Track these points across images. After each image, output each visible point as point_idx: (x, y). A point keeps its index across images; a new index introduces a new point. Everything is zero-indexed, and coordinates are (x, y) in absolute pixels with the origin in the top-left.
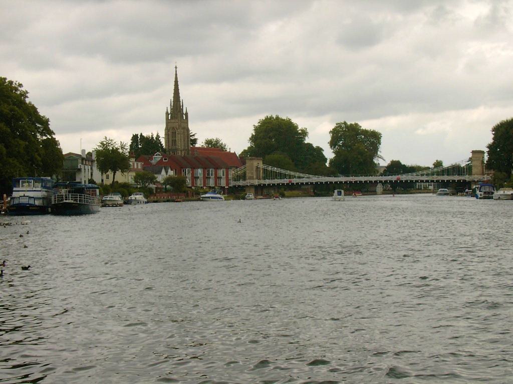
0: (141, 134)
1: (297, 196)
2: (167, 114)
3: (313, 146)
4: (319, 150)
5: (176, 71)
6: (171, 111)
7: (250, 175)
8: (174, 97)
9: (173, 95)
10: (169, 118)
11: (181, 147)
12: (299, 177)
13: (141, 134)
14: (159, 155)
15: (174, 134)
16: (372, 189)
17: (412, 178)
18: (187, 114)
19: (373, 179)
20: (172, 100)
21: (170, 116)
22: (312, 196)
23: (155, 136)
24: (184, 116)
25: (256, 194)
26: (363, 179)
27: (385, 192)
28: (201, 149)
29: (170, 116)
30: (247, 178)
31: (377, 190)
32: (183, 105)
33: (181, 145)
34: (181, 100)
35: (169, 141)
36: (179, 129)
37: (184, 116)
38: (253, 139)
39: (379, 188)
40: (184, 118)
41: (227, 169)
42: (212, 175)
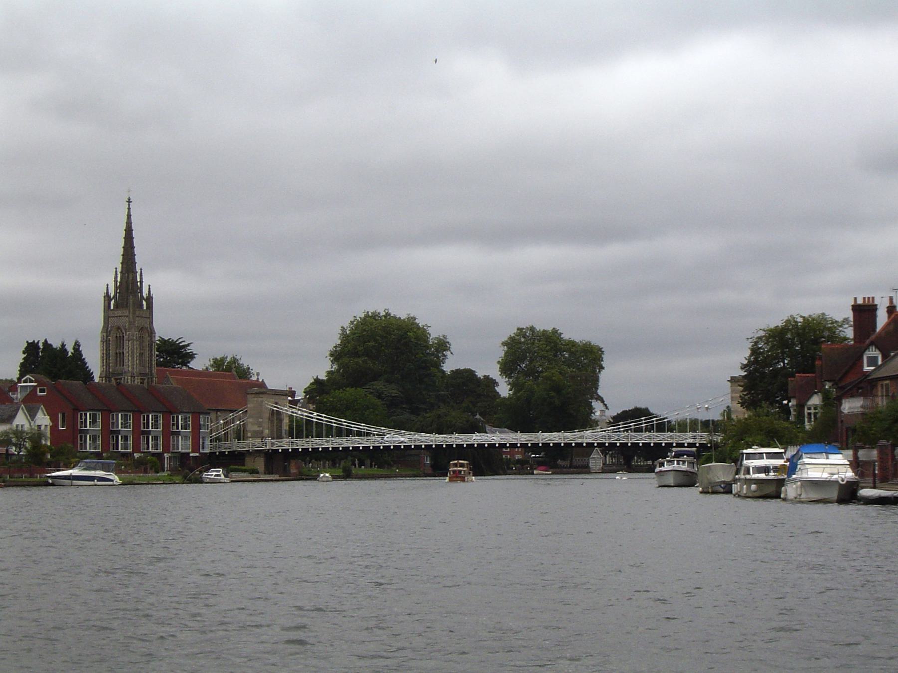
0: (46, 341)
1: (396, 476)
2: (107, 297)
3: (476, 376)
4: (490, 383)
5: (129, 209)
6: (116, 293)
7: (256, 428)
8: (122, 263)
9: (120, 259)
10: (112, 308)
11: (133, 368)
12: (359, 434)
13: (46, 341)
14: (31, 381)
15: (120, 340)
16: (577, 461)
17: (603, 437)
18: (149, 299)
19: (587, 436)
20: (119, 270)
21: (113, 302)
22: (427, 475)
23: (70, 350)
24: (144, 303)
25: (269, 470)
26: (295, 430)
27: (608, 469)
28: (204, 373)
29: (113, 302)
30: (249, 435)
31: (590, 465)
32: (141, 278)
33: (133, 365)
34: (138, 270)
35: (108, 355)
36: (129, 329)
37: (144, 303)
38: (337, 356)
39: (596, 460)
40: (145, 308)
41: (196, 414)
42: (185, 427)
